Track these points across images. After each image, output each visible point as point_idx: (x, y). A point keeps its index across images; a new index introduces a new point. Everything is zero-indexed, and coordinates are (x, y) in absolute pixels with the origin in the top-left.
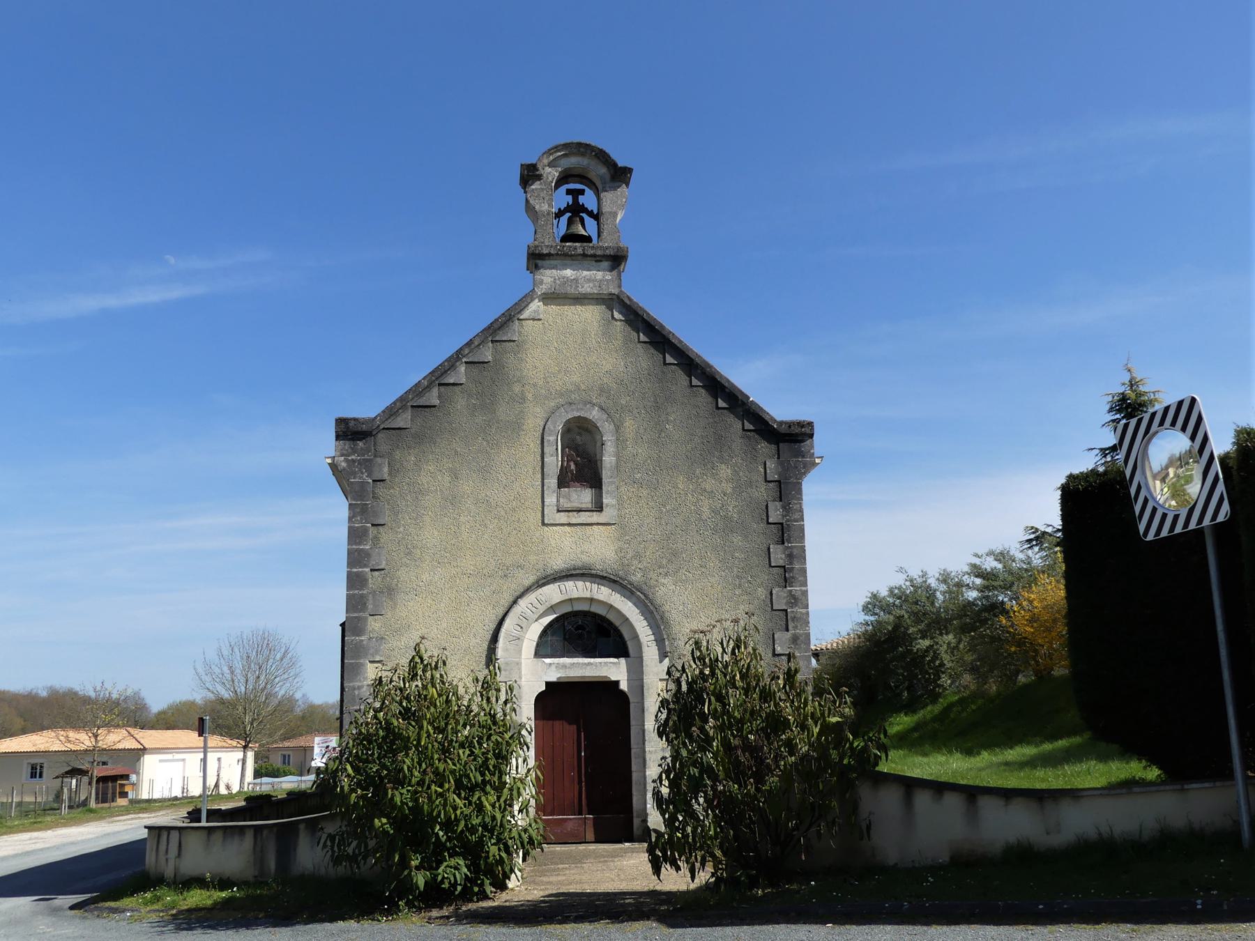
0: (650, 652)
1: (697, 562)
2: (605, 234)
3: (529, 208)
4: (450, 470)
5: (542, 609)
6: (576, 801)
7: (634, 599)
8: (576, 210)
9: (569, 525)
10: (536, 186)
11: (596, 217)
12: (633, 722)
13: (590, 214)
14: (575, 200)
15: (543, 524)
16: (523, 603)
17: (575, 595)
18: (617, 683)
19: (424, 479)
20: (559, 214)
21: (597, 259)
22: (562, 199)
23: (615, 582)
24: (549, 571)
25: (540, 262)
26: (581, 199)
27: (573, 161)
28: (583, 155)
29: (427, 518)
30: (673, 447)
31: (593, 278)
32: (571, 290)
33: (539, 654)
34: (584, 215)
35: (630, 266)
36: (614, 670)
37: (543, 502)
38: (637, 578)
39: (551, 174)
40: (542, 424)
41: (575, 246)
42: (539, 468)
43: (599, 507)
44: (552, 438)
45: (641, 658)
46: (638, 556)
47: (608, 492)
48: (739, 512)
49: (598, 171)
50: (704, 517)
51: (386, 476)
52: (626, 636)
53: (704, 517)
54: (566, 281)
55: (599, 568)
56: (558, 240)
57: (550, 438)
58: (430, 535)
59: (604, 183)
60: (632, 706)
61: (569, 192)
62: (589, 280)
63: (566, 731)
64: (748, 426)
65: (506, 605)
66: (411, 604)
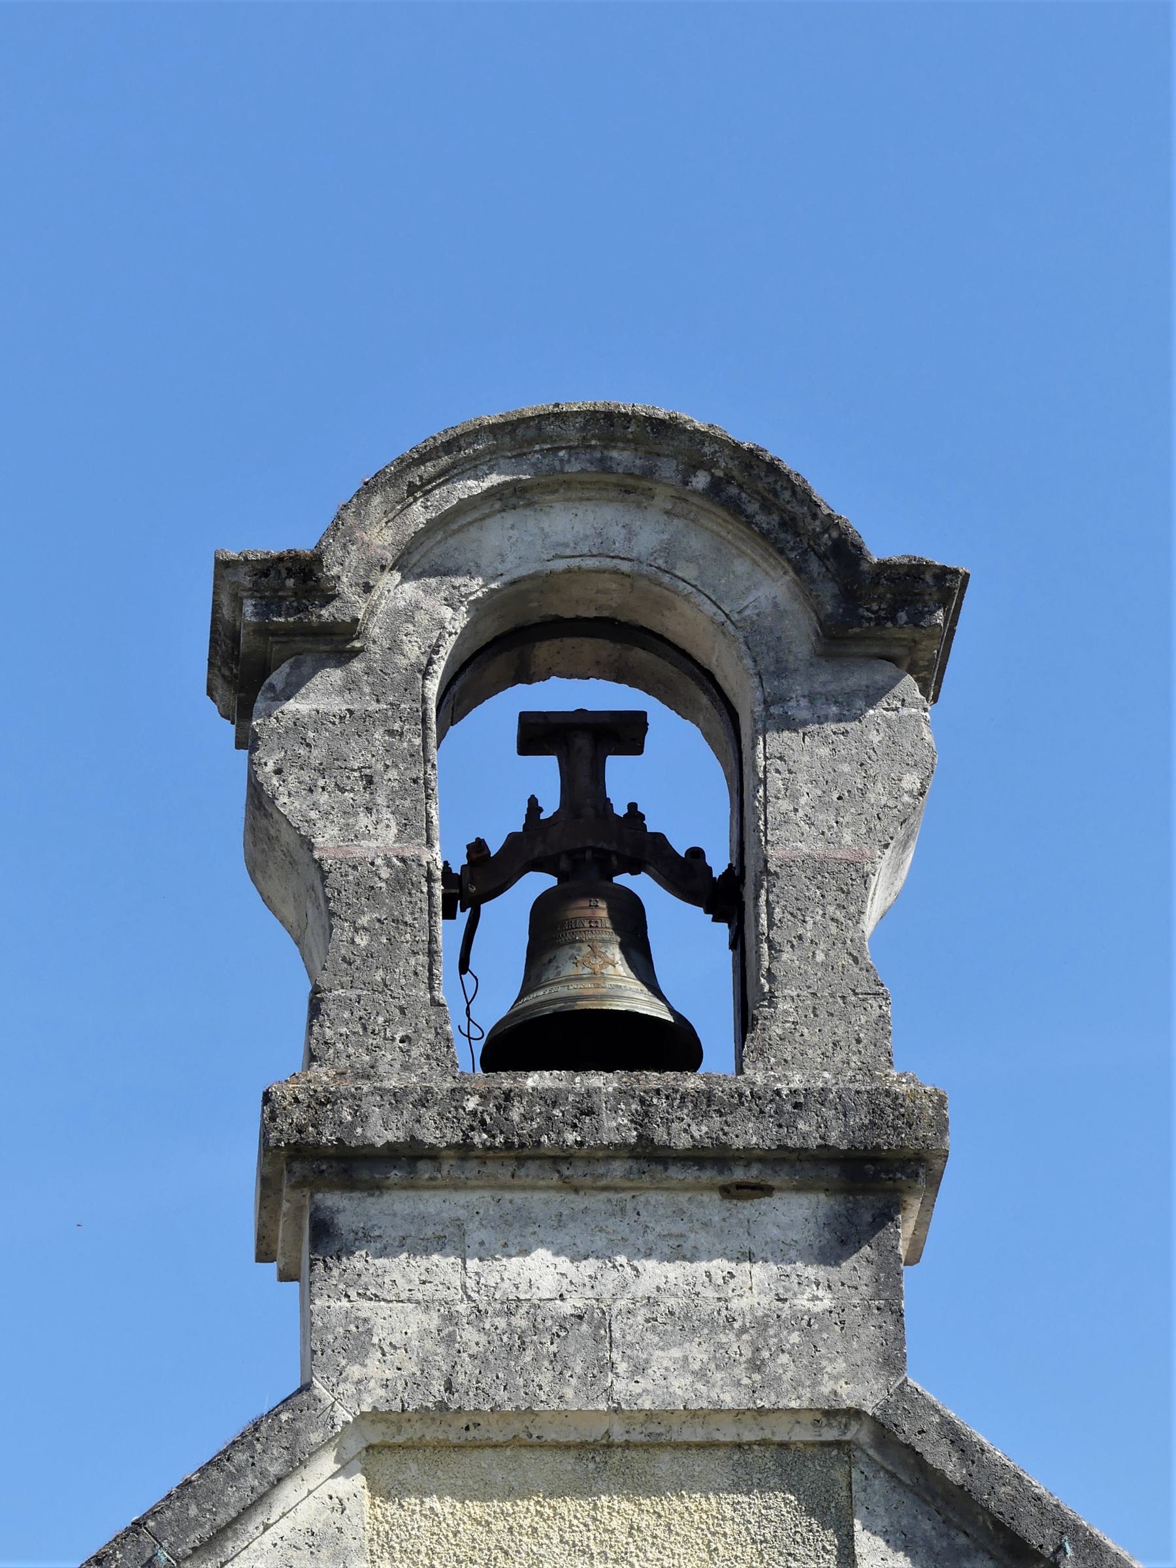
2: (784, 1012)
3: (271, 844)
8: (586, 855)
10: (319, 697)
11: (724, 896)
13: (686, 875)
14: (582, 786)
20: (472, 884)
21: (737, 1175)
22: (494, 783)
25: (347, 1209)
26: (623, 781)
27: (566, 536)
28: (631, 489)
31: (707, 1310)
32: (561, 1394)
34: (641, 885)
35: (953, 1223)
39: (420, 618)
41: (587, 1086)
49: (737, 594)
54: (528, 1330)
56: (467, 1056)
59: (773, 670)
61: (536, 734)
62: (684, 1323)
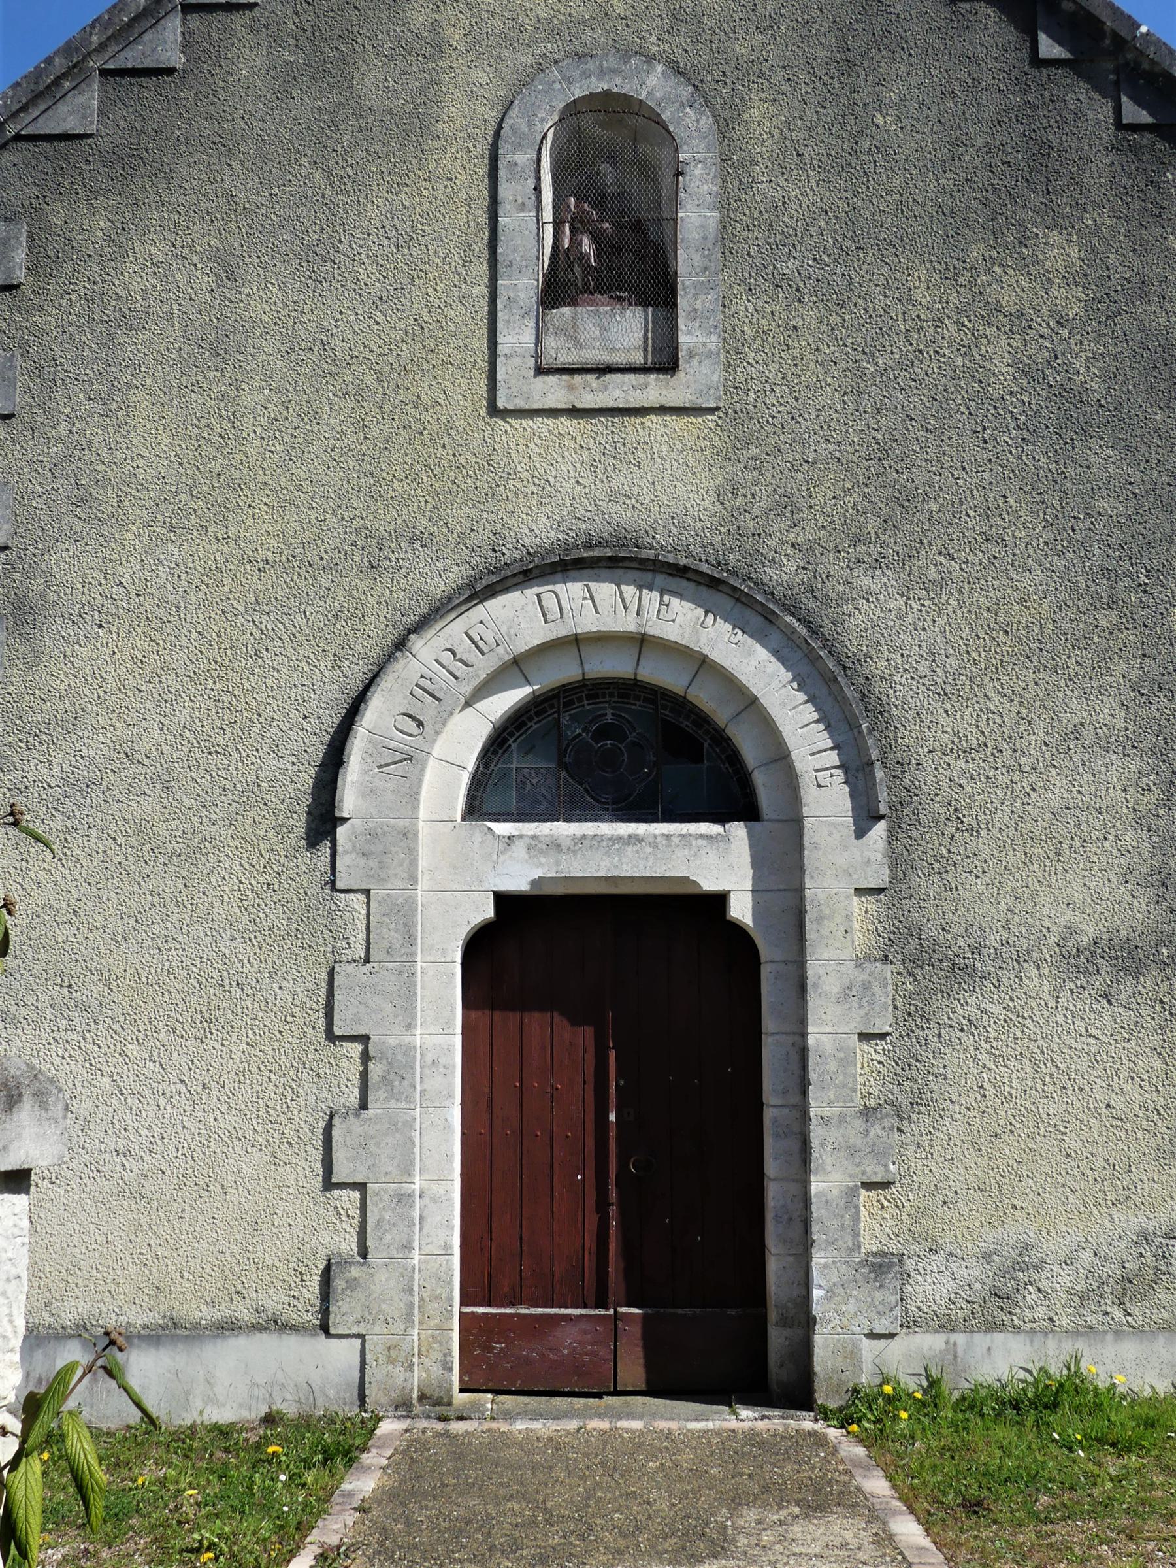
0: (826, 802)
1: (973, 526)
4: (215, 256)
5: (484, 667)
6: (589, 1263)
7: (775, 637)
9: (574, 412)
12: (769, 1023)
15: (494, 410)
16: (427, 649)
17: (589, 623)
18: (720, 900)
19: (133, 283)
23: (713, 583)
24: (509, 554)
29: (139, 398)
30: (897, 181)
33: (477, 807)
36: (712, 859)
37: (493, 344)
38: (783, 574)
40: (493, 116)
42: (481, 247)
43: (665, 360)
44: (524, 158)
45: (795, 823)
46: (785, 505)
47: (693, 314)
48: (1108, 377)
50: (996, 390)
51: (20, 275)
52: (750, 753)
53: (996, 390)
55: (663, 540)
57: (516, 158)
58: (149, 445)
60: (766, 972)
63: (561, 1043)
64: (1133, 113)
65: (375, 654)
66: (84, 652)
